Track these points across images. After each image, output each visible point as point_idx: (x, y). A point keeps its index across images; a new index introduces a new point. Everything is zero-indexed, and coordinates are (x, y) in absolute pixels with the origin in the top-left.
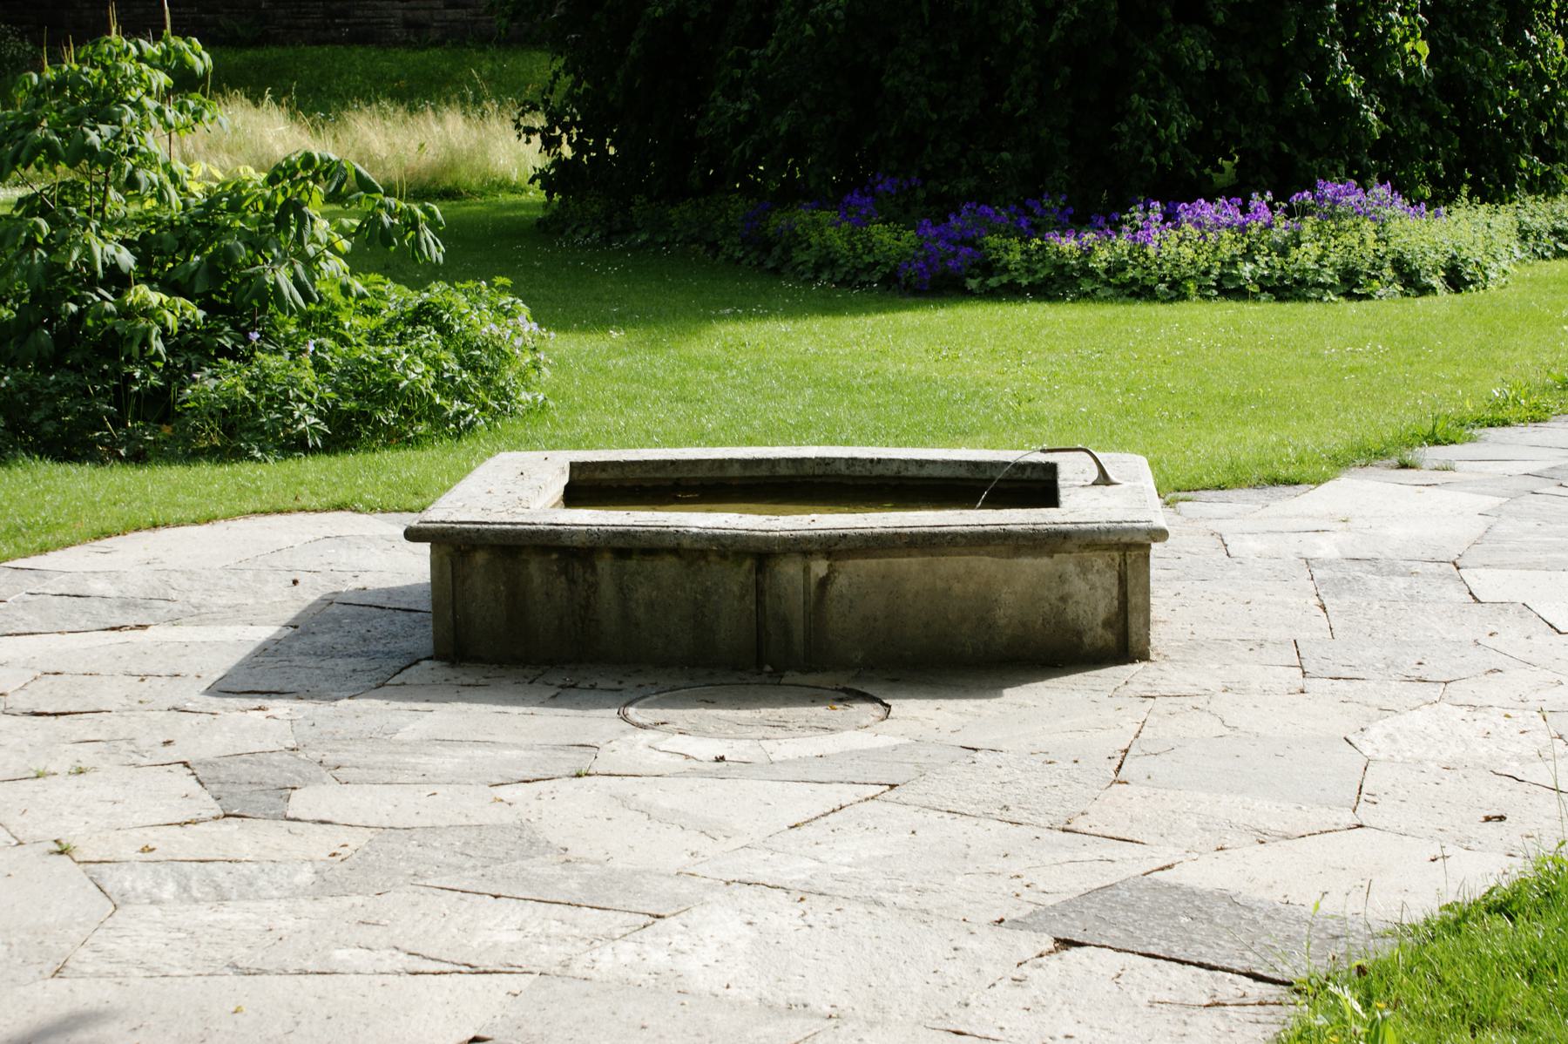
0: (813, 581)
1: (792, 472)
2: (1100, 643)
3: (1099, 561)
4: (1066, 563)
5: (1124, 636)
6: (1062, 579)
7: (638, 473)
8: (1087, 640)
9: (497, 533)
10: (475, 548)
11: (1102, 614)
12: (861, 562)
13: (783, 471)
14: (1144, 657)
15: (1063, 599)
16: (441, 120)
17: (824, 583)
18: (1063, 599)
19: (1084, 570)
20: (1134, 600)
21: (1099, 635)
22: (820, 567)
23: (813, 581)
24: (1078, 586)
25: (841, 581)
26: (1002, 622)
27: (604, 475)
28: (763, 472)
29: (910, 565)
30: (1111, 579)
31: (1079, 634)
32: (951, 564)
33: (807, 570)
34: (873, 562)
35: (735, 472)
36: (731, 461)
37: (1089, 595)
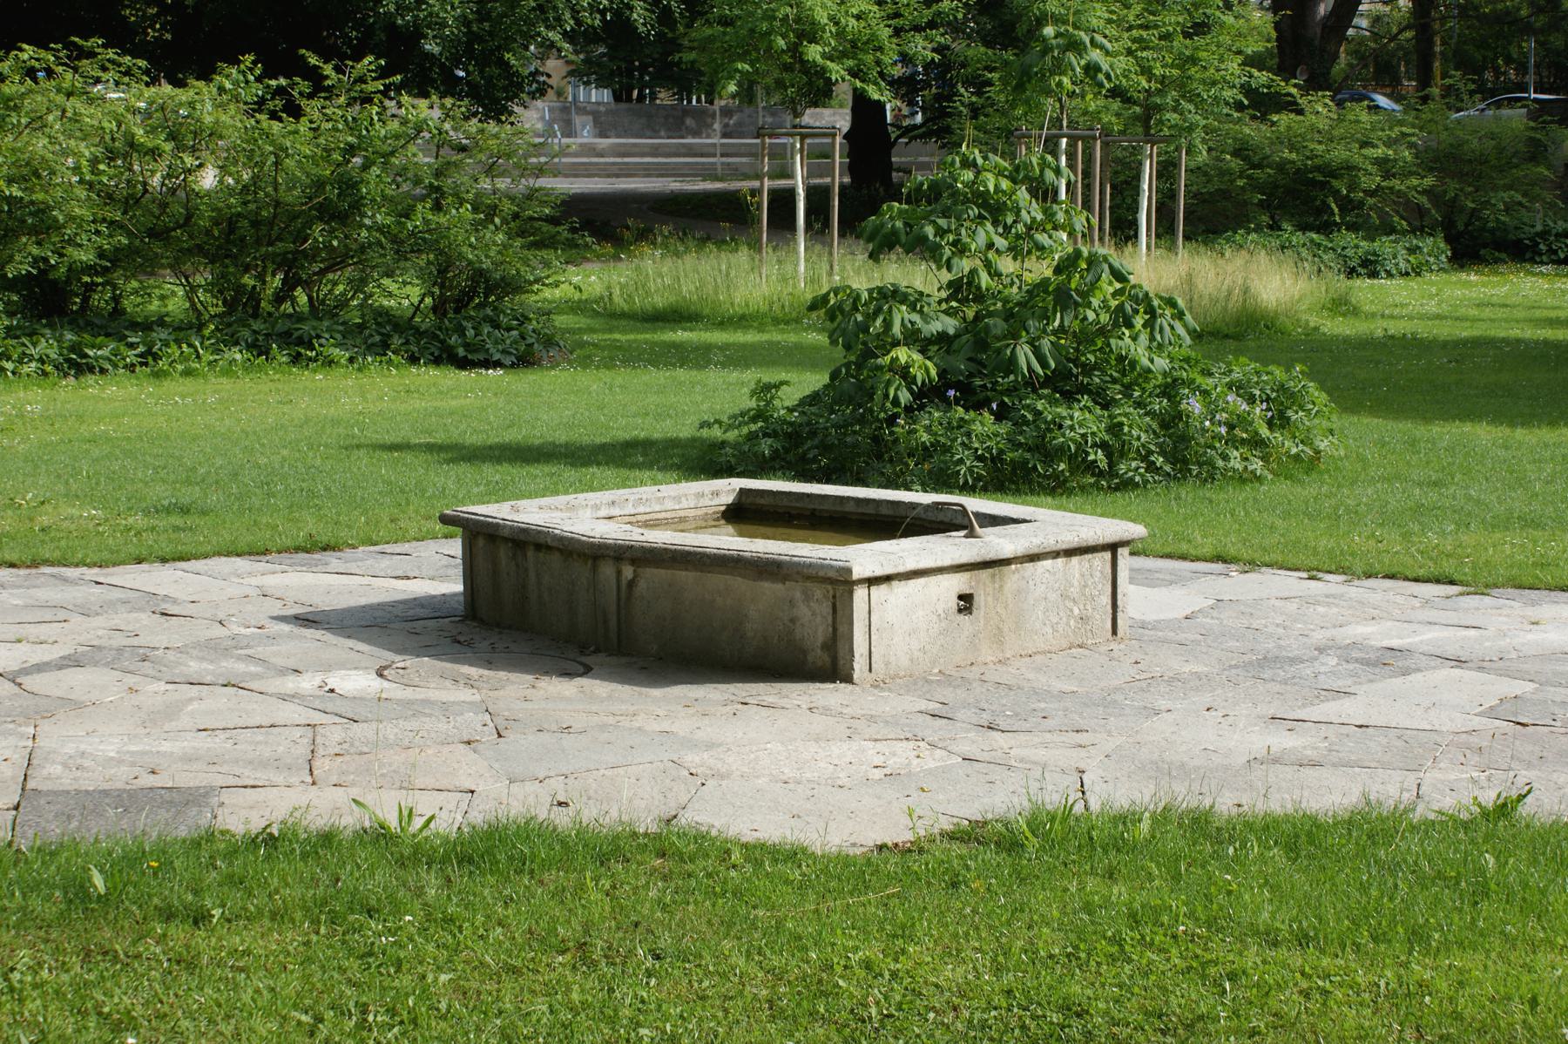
0: (624, 583)
1: (890, 512)
2: (820, 664)
3: (818, 592)
4: (795, 590)
5: (834, 660)
6: (792, 603)
7: (785, 502)
8: (810, 658)
9: (561, 539)
10: (603, 557)
11: (820, 639)
12: (656, 571)
13: (884, 511)
14: (848, 679)
15: (793, 621)
16: (717, 258)
17: (631, 584)
18: (793, 621)
19: (808, 598)
20: (842, 629)
21: (818, 657)
22: (628, 572)
23: (624, 583)
24: (803, 611)
25: (642, 585)
26: (750, 634)
27: (762, 501)
28: (870, 510)
29: (686, 577)
30: (826, 608)
31: (804, 652)
32: (717, 580)
33: (619, 573)
34: (663, 571)
35: (850, 508)
36: (849, 498)
37: (812, 621)
